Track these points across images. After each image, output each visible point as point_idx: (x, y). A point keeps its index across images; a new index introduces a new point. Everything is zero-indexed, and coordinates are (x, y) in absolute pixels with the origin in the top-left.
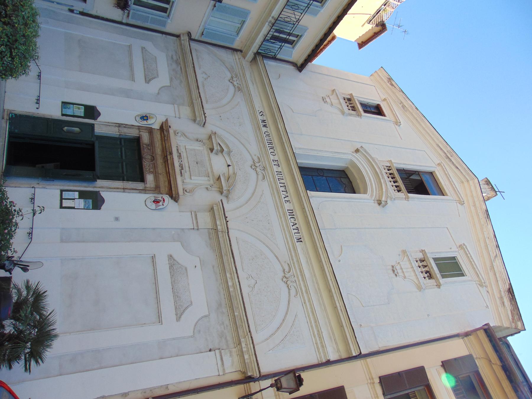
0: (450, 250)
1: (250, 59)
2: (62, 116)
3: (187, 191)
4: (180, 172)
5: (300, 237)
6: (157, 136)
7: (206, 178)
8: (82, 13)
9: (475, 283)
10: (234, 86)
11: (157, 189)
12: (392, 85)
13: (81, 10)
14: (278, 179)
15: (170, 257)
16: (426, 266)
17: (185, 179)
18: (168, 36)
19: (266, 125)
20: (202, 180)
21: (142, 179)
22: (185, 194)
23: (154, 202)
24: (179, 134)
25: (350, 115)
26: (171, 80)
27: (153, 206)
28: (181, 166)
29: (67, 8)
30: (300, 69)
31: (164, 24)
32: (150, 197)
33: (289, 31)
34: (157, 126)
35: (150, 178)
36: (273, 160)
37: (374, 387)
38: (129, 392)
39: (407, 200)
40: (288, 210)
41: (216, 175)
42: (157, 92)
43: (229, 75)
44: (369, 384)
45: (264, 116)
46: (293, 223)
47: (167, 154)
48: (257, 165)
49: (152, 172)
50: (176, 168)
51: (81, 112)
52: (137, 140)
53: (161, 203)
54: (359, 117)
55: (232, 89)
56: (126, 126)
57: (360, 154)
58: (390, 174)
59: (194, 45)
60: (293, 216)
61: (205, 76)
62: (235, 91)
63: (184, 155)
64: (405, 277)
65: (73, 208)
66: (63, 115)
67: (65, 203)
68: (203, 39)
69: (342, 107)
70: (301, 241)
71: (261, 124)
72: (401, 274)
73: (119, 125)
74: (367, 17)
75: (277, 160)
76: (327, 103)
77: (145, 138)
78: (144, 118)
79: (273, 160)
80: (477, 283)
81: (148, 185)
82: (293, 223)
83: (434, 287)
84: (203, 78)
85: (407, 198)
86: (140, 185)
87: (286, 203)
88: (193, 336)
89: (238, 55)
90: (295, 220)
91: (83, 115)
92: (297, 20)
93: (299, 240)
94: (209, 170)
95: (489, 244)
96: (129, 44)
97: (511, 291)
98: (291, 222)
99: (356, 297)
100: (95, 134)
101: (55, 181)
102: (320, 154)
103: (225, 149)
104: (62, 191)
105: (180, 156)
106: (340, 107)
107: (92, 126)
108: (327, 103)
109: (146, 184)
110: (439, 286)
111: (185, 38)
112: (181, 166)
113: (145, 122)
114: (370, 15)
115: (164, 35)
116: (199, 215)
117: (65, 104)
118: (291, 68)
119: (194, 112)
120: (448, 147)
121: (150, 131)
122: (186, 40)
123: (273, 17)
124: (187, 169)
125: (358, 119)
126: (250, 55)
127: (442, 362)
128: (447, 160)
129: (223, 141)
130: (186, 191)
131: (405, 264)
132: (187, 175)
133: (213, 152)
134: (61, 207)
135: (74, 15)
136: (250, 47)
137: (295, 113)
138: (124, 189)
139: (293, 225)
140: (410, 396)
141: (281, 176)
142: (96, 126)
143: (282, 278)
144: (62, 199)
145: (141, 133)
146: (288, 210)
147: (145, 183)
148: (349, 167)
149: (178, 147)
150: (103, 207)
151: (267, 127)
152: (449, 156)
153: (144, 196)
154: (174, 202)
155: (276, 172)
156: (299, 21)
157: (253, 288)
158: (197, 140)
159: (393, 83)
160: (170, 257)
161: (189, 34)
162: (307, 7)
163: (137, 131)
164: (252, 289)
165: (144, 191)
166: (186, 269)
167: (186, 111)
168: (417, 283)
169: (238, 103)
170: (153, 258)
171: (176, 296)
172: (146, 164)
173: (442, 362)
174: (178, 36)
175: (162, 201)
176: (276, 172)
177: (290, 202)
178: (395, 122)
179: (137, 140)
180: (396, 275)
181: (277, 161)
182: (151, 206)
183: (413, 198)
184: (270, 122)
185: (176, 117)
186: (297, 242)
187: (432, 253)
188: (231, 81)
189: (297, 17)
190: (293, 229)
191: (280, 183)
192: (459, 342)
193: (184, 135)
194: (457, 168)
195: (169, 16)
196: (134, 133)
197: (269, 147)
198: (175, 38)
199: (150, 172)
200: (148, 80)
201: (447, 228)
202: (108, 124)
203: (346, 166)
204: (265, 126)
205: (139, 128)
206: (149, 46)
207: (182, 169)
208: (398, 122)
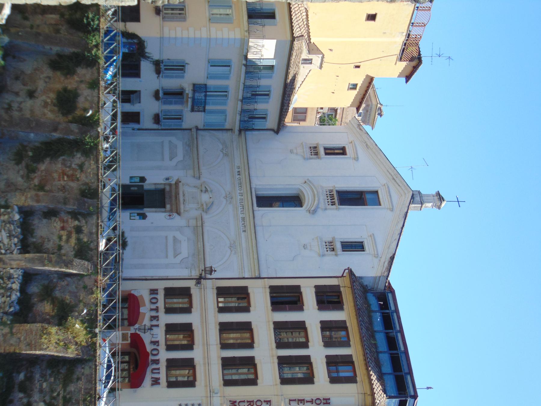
2: (165, 360)
6: (174, 187)
8: (139, 129)
12: (360, 129)
13: (138, 128)
15: (174, 237)
16: (332, 245)
21: (164, 207)
26: (184, 156)
28: (184, 200)
29: (131, 129)
31: (181, 125)
32: (168, 214)
34: (173, 182)
35: (168, 206)
47: (177, 194)
48: (228, 196)
49: (169, 204)
51: (138, 180)
53: (172, 216)
55: (221, 155)
56: (158, 184)
64: (311, 250)
65: (135, 219)
66: (130, 182)
67: (132, 218)
68: (205, 128)
71: (236, 173)
73: (155, 184)
74: (395, 58)
77: (168, 188)
78: (167, 179)
86: (163, 210)
89: (229, 133)
91: (138, 181)
93: (244, 231)
96: (162, 141)
97: (392, 258)
100: (144, 189)
101: (130, 123)
102: (275, 187)
103: (209, 189)
104: (130, 213)
105: (184, 195)
107: (142, 186)
112: (184, 200)
113: (168, 181)
114: (397, 56)
117: (131, 178)
118: (272, 132)
120: (395, 171)
121: (170, 185)
123: (239, 111)
126: (237, 132)
128: (393, 181)
134: (130, 219)
135: (135, 131)
138: (156, 212)
142: (144, 186)
144: (130, 216)
145: (165, 187)
150: (147, 219)
152: (395, 178)
153: (164, 214)
158: (195, 187)
159: (361, 127)
160: (174, 237)
165: (165, 212)
167: (190, 172)
170: (166, 237)
171: (175, 250)
174: (190, 129)
184: (242, 172)
192: (336, 279)
194: (399, 186)
196: (162, 187)
198: (189, 131)
200: (171, 159)
202: (150, 184)
203: (298, 193)
205: (165, 184)
206: (174, 139)
207: (184, 201)
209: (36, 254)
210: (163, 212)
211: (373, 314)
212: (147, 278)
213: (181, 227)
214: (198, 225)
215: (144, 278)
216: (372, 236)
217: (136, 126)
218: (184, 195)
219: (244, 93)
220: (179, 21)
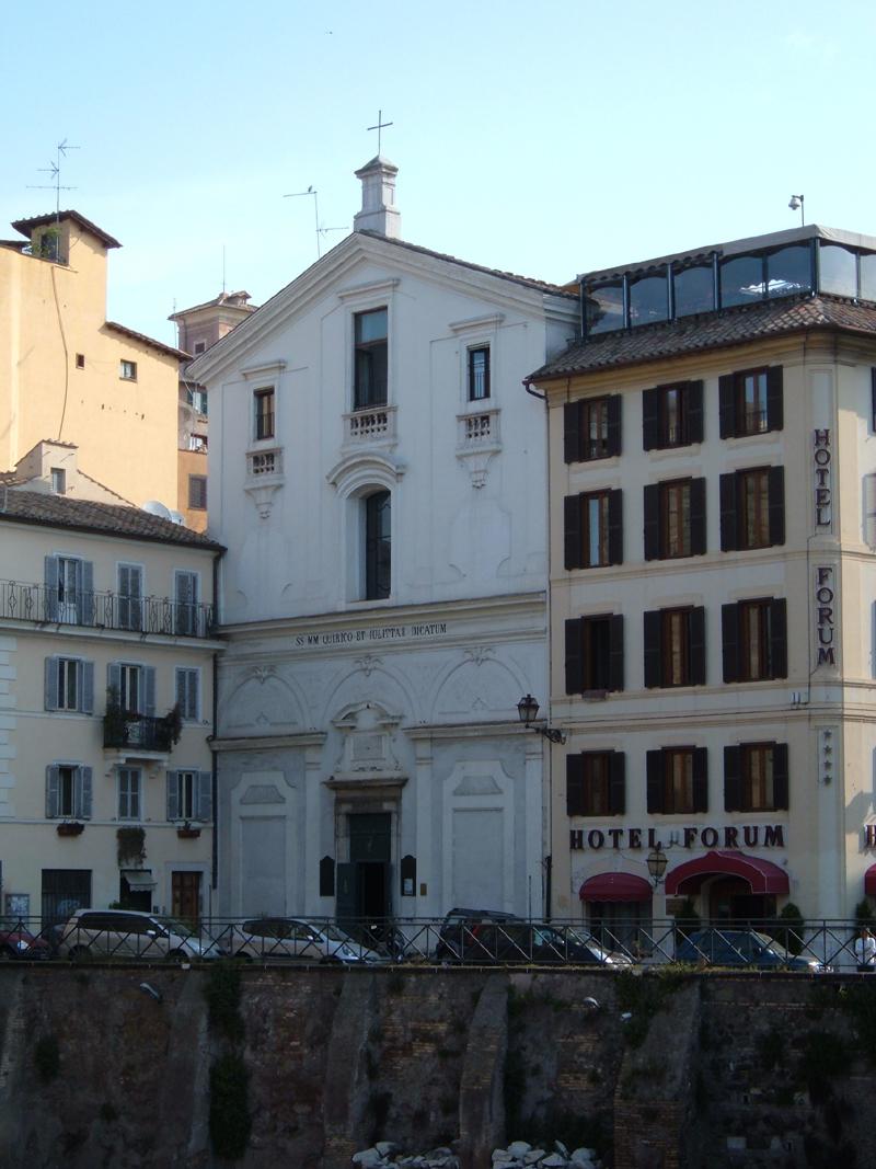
11: (397, 800)
15: (456, 793)
18: (218, 766)
20: (386, 744)
21: (388, 815)
26: (275, 769)
31: (205, 776)
35: (387, 806)
40: (472, 397)
50: (376, 778)
52: (351, 817)
61: (262, 720)
62: (276, 677)
72: (480, 476)
77: (346, 808)
85: (394, 409)
86: (394, 818)
93: (443, 628)
94: (374, 734)
99: (449, 675)
104: (403, 894)
107: (340, 865)
111: (216, 745)
116: (419, 755)
119: (309, 746)
121: (339, 802)
129: (339, 714)
131: (472, 463)
132: (379, 764)
136: (209, 649)
138: (398, 835)
140: (571, 312)
146: (472, 397)
154: (407, 785)
160: (456, 793)
167: (311, 755)
179: (350, 816)
188: (263, 680)
195: (194, 772)
196: (342, 820)
199: (381, 806)
200: (282, 800)
206: (236, 796)
216: (456, 330)
217: (207, 880)
218: (363, 769)
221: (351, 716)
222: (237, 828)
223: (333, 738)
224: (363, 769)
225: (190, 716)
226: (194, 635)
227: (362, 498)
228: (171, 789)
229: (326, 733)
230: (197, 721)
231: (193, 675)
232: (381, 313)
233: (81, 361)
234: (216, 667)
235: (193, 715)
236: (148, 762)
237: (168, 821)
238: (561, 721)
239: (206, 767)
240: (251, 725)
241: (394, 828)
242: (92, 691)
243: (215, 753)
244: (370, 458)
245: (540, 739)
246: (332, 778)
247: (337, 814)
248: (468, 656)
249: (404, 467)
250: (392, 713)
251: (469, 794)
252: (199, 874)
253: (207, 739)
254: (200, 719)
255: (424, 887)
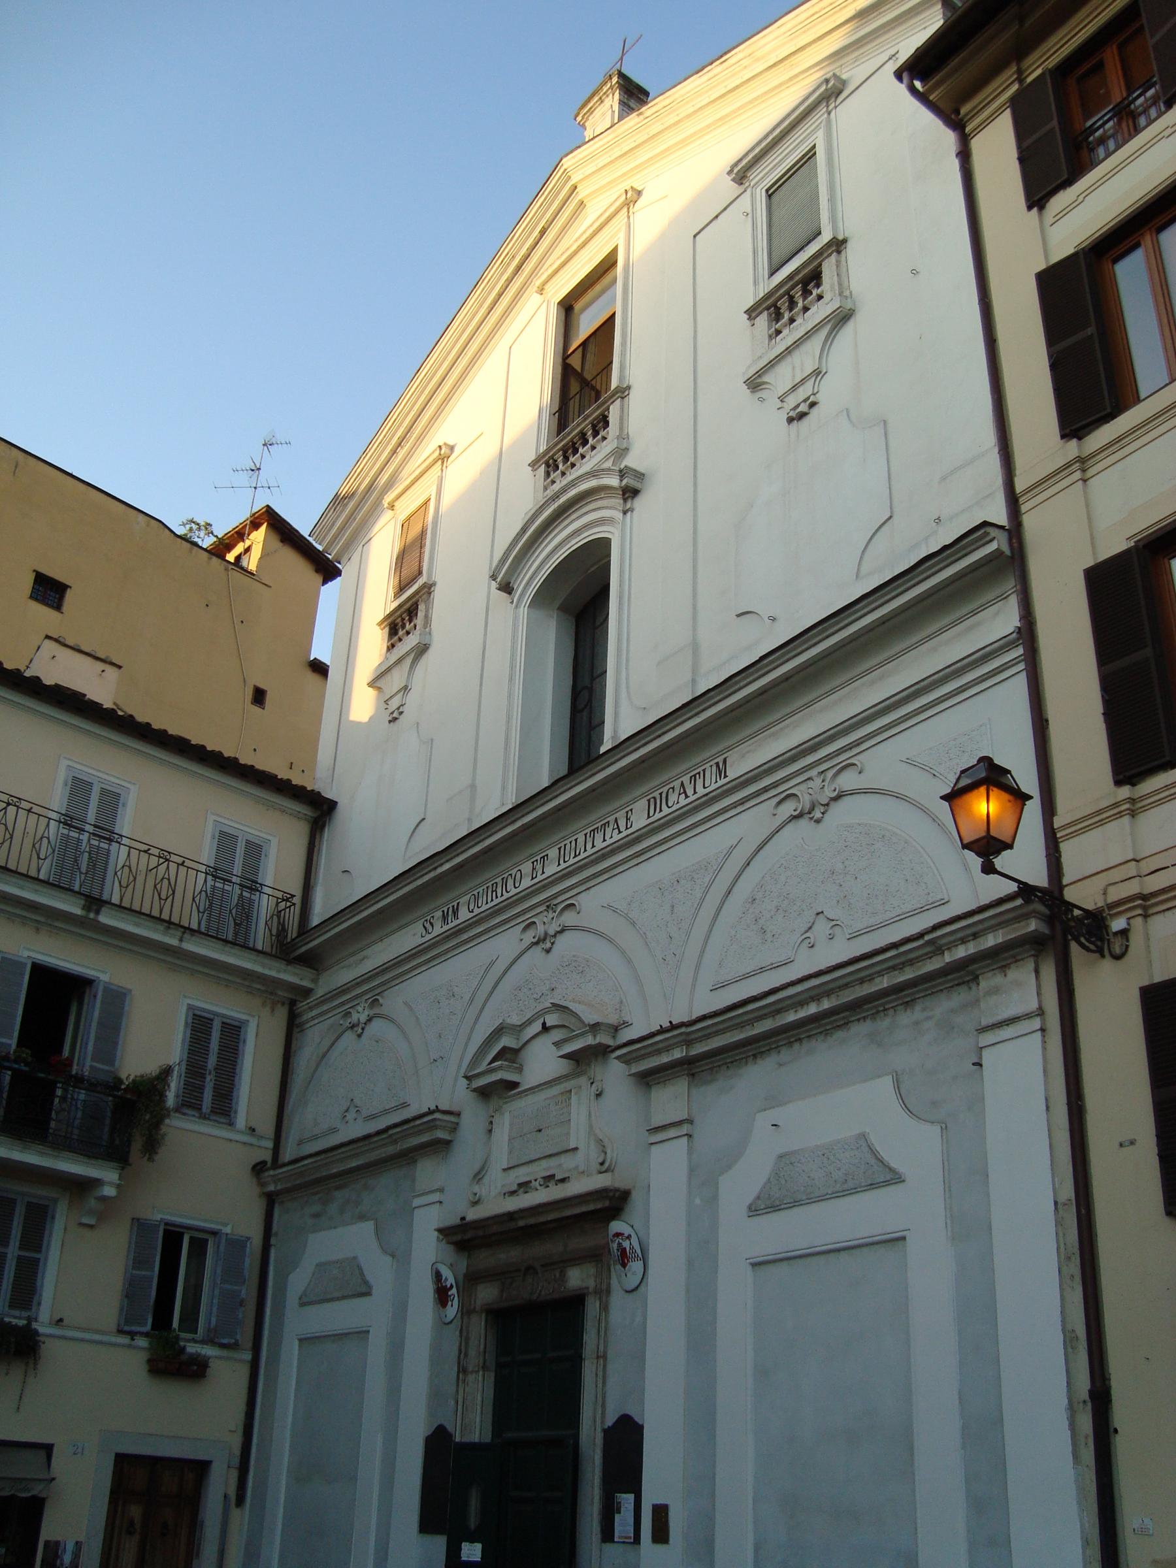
0: (750, 215)
1: (308, 973)
3: (601, 1160)
4: (560, 1185)
5: (714, 768)
6: (488, 1259)
7: (574, 1098)
9: (833, 114)
10: (370, 1020)
14: (576, 856)
15: (754, 1210)
17: (577, 1167)
19: (453, 906)
20: (580, 1109)
21: (577, 1301)
22: (609, 1166)
23: (624, 1265)
24: (476, 1189)
25: (427, 619)
26: (362, 1217)
27: (636, 1266)
30: (325, 807)
31: (237, 1245)
33: (202, 876)
35: (577, 1278)
36: (533, 879)
37: (1093, 455)
38: (1064, 1330)
39: (627, 393)
41: (563, 1067)
42: (389, 1259)
43: (349, 1036)
44: (1090, 473)
45: (433, 917)
46: (680, 794)
49: (563, 1274)
52: (498, 1316)
53: (626, 1244)
54: (432, 589)
55: (377, 1026)
56: (463, 1353)
57: (514, 579)
58: (566, 459)
59: (288, 1154)
60: (664, 795)
63: (522, 1174)
69: (407, 654)
70: (725, 761)
75: (533, 863)
76: (402, 705)
77: (487, 1294)
79: (533, 879)
80: (833, 105)
81: (591, 1283)
82: (680, 794)
83: (843, 259)
84: (355, 1119)
86: (592, 1306)
87: (631, 827)
88: (944, 1126)
90: (673, 788)
92: (162, 860)
95: (678, 115)
98: (678, 803)
106: (409, 661)
108: (402, 705)
109: (588, 1288)
110: (838, 245)
115: (273, 1241)
121: (471, 1280)
122: (273, 1176)
124: (553, 1162)
125: (438, 595)
127: (1030, 208)
130: (602, 1164)
132: (567, 1163)
133: (518, 1081)
137: (425, 815)
138: (602, 1357)
139: (617, 830)
141: (568, 847)
143: (812, 822)
145: (478, 1308)
147: (586, 1291)
148: (557, 603)
149: (505, 1194)
151: (458, 904)
155: (559, 864)
156: (166, 854)
157: (834, 923)
158: (490, 1131)
160: (754, 1210)
161: (258, 1169)
162: (119, 840)
163: (475, 1318)
164: (837, 927)
165: (603, 1292)
166: (781, 1157)
167: (427, 1172)
168: (829, 327)
169: (406, 1003)
172: (541, 1289)
173: (1030, 208)
175: (621, 1241)
176: (559, 864)
177: (630, 812)
178: (443, 463)
180: (813, 405)
181: (535, 863)
182: (634, 1273)
183: (622, 378)
185: (441, 1202)
186: (726, 776)
187: (755, 283)
189: (154, 861)
190: (695, 792)
191: (585, 850)
193: (479, 1172)
195: (214, 1233)
196: (478, 1325)
197: (502, 895)
201: (697, 237)
204: (455, 912)
205: (466, 1312)
206: (299, 1281)
207: (552, 1177)
208: (440, 454)
209: (30, 1494)
210: (605, 1308)
211: (179, 933)
212: (1084, 1383)
213: (692, 1170)
214: (1143, 863)
215: (1086, 1423)
217: (220, 1483)
218: (525, 1186)
219: (192, 873)
220: (970, 670)
221: (510, 1055)
222: (291, 1351)
223: (472, 1117)
224: (525, 1186)
225: (214, 1111)
226: (241, 943)
227: (558, 609)
228: (139, 1261)
229: (458, 1114)
230: (231, 1124)
231: (233, 1033)
232: (900, 1243)
233: (259, 697)
234: (293, 1027)
235: (223, 1108)
236: (81, 1187)
237: (120, 1331)
238: (1100, 882)
239: (253, 1230)
240: (333, 1130)
241: (590, 1339)
242: (268, 1205)
243: (271, 1200)
244: (572, 493)
245: (1030, 965)
246: (463, 1219)
247: (209, 1119)
248: (789, 808)
249: (640, 476)
250: (590, 1017)
251: (796, 1203)
252: (201, 1467)
253: (254, 1167)
254: (241, 1121)
255: (661, 1513)
